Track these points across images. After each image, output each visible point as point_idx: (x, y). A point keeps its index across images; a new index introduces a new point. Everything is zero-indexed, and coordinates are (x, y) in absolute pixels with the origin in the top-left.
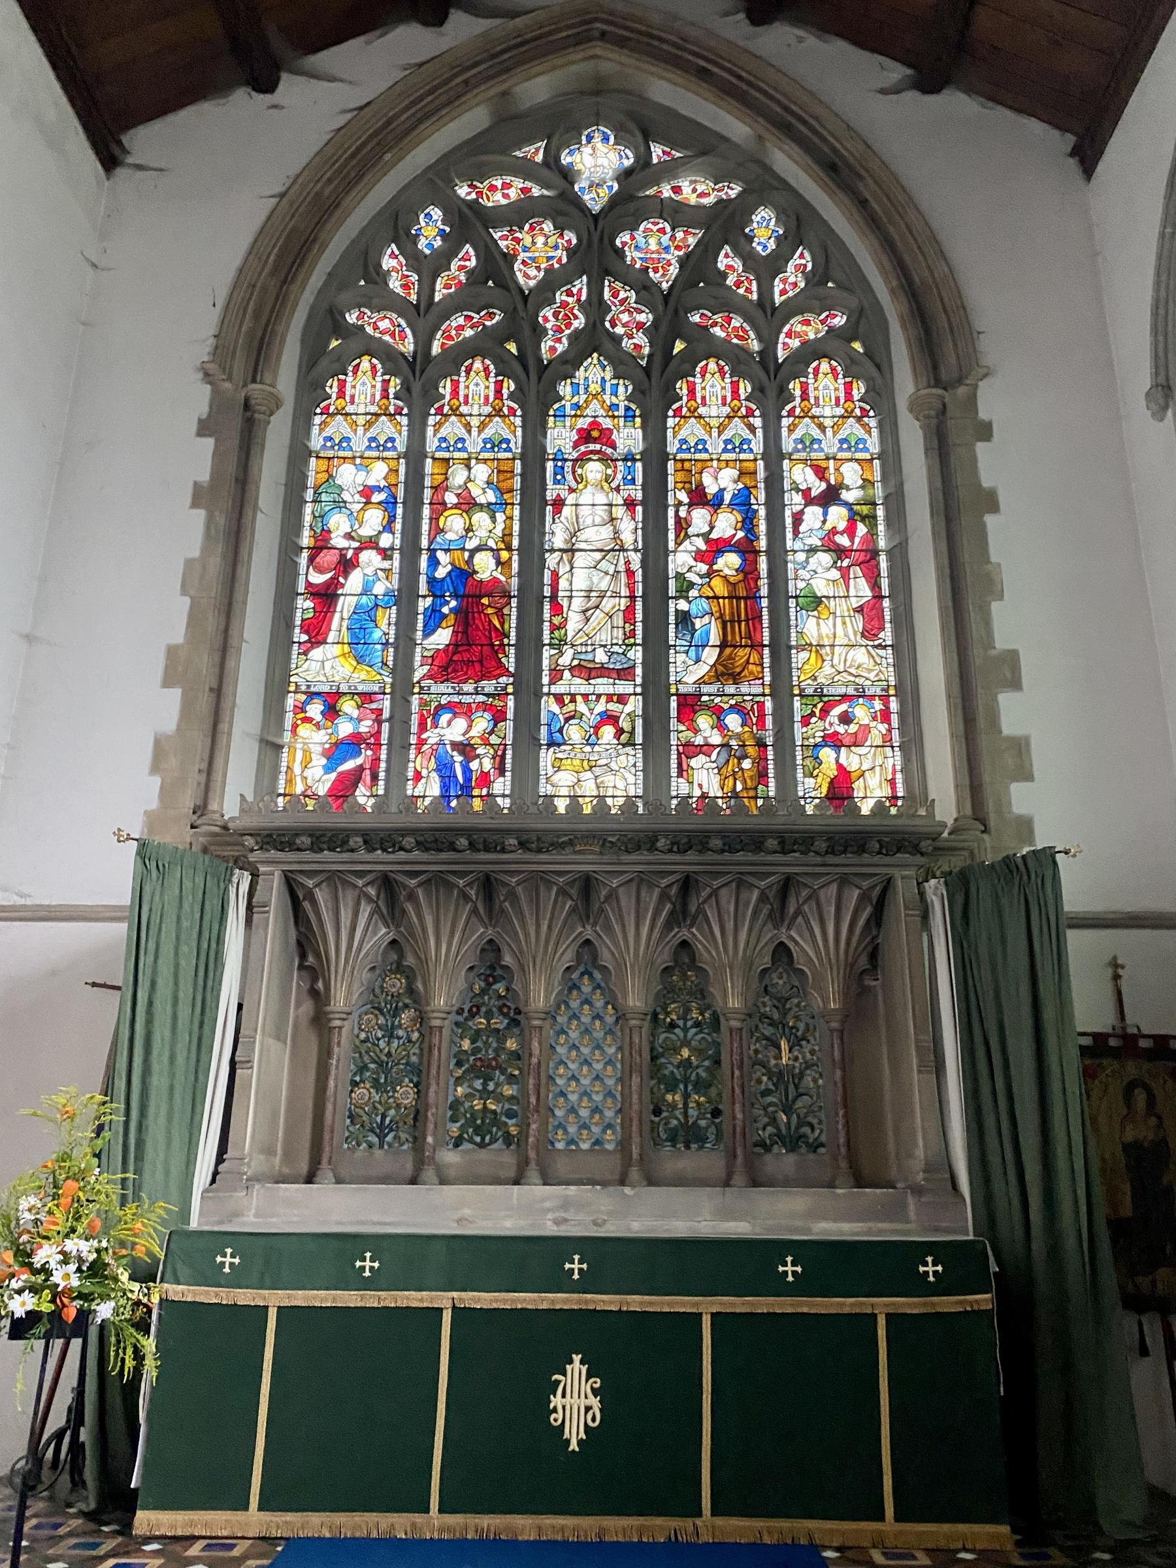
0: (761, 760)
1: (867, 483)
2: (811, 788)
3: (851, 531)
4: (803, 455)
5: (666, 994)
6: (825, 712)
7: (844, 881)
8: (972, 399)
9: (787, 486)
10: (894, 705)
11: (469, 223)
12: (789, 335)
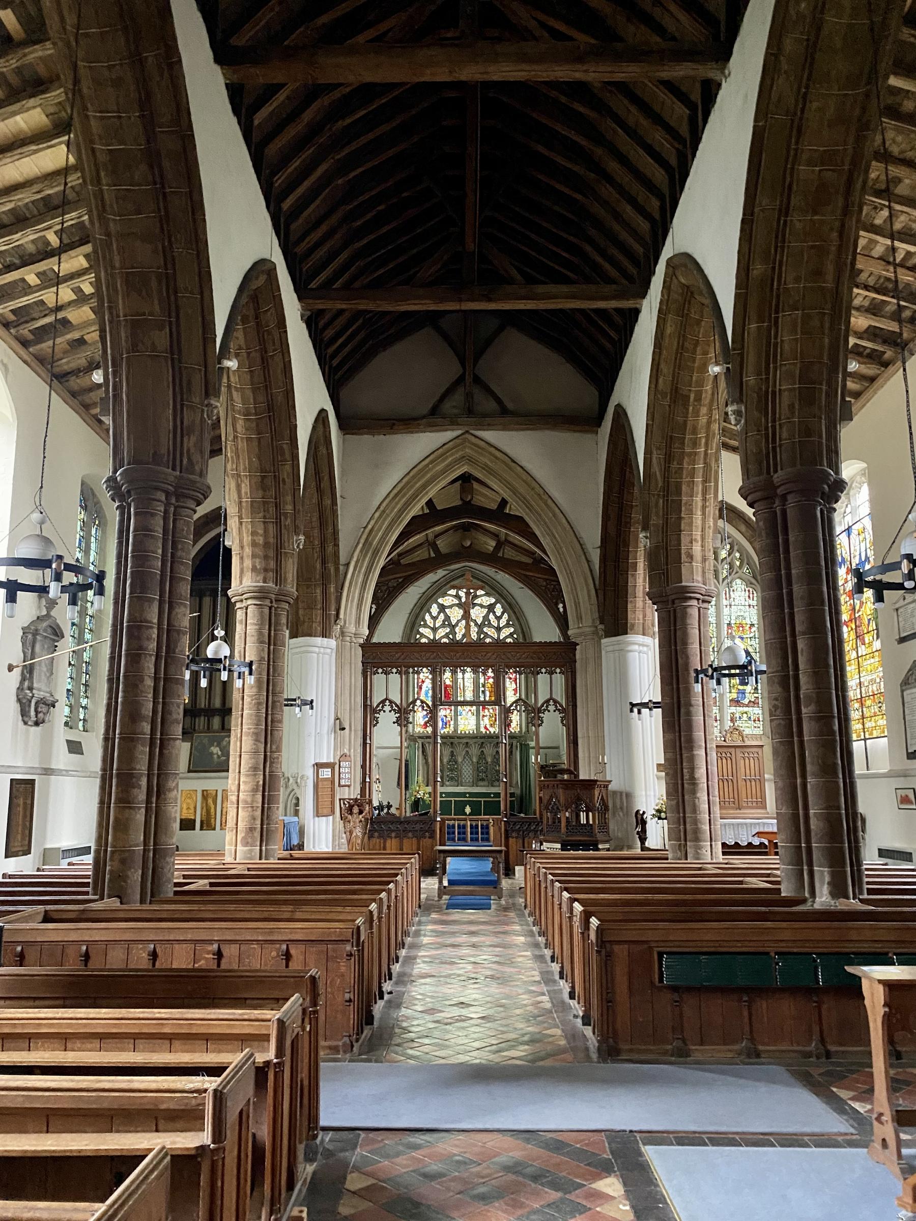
5: (480, 758)
11: (442, 608)
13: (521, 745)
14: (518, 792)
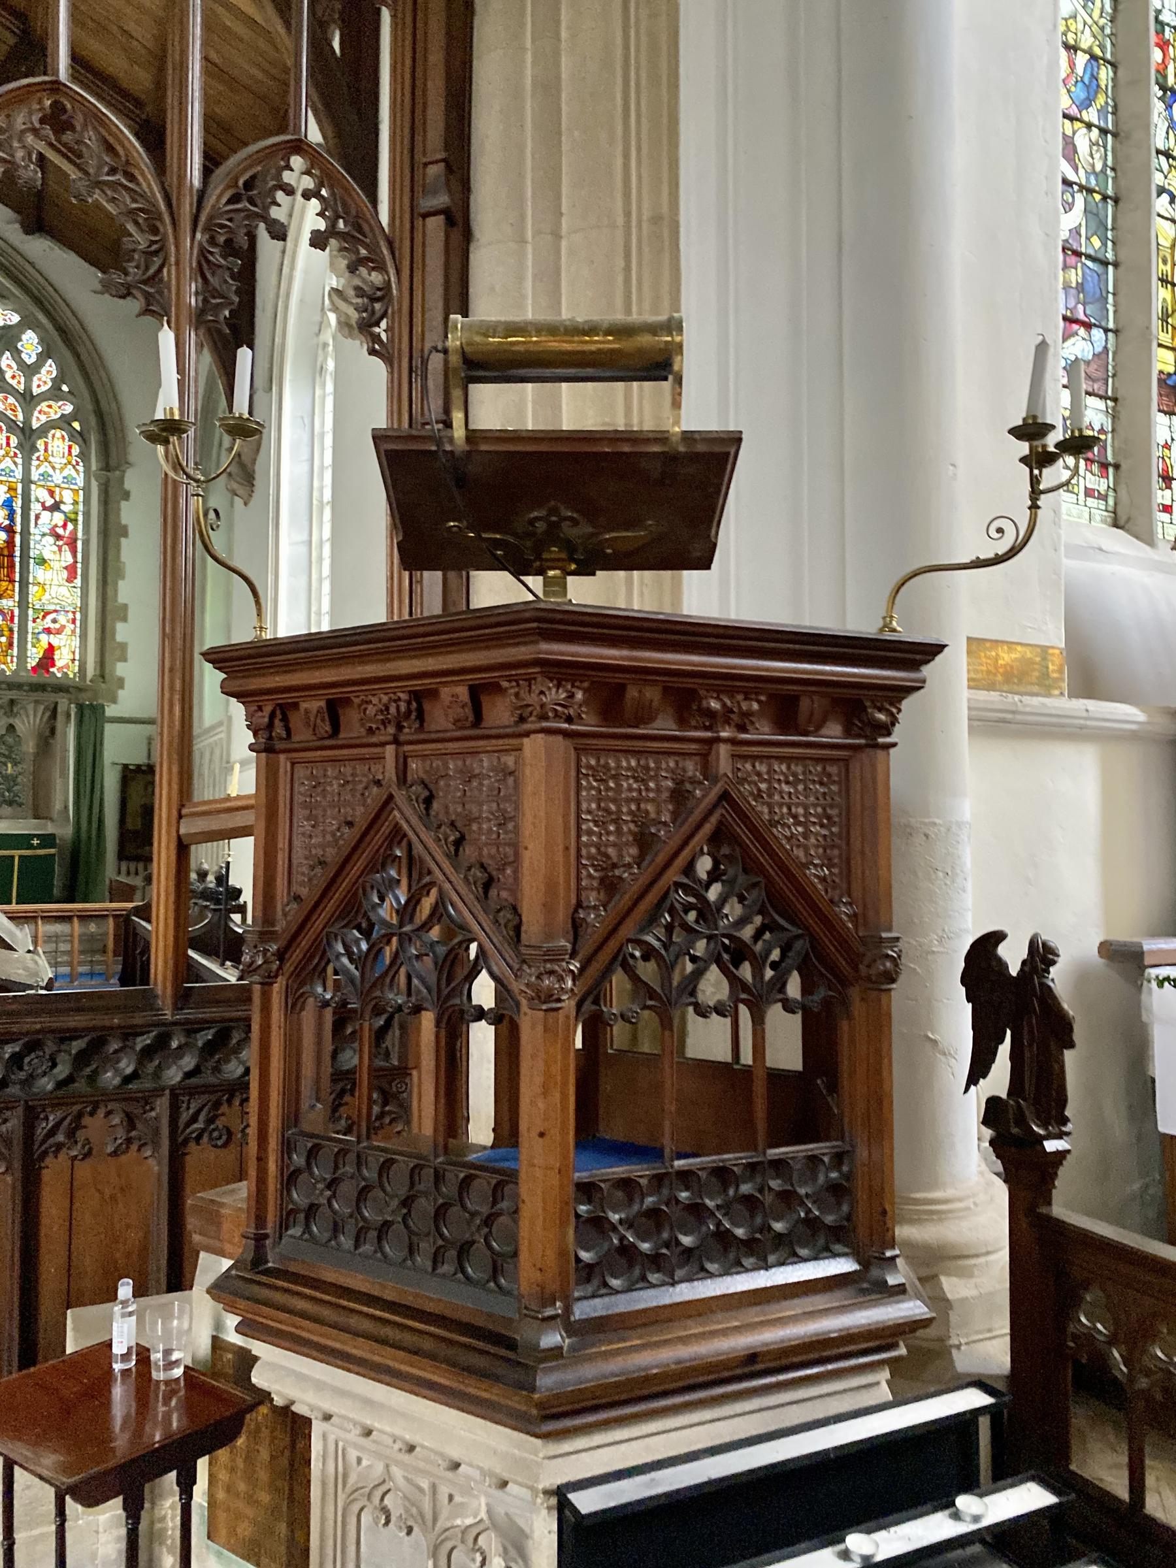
0: (10, 638)
1: (75, 503)
2: (34, 655)
3: (65, 526)
4: (42, 483)
6: (44, 617)
7: (37, 702)
8: (121, 480)
9: (33, 499)
10: (78, 616)
12: (40, 412)
13: (81, 707)
14: (65, 832)
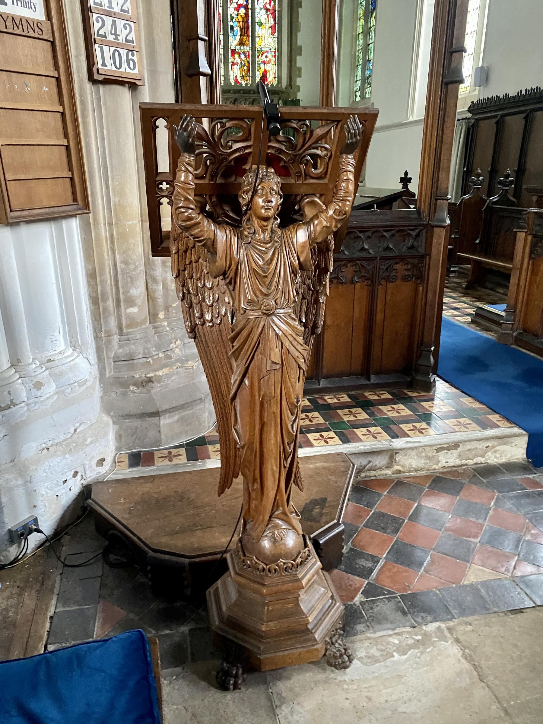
6: (262, 55)
